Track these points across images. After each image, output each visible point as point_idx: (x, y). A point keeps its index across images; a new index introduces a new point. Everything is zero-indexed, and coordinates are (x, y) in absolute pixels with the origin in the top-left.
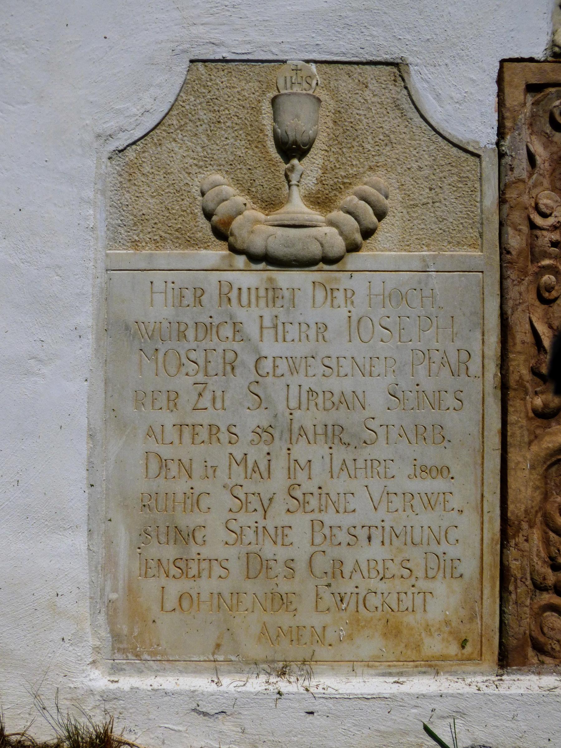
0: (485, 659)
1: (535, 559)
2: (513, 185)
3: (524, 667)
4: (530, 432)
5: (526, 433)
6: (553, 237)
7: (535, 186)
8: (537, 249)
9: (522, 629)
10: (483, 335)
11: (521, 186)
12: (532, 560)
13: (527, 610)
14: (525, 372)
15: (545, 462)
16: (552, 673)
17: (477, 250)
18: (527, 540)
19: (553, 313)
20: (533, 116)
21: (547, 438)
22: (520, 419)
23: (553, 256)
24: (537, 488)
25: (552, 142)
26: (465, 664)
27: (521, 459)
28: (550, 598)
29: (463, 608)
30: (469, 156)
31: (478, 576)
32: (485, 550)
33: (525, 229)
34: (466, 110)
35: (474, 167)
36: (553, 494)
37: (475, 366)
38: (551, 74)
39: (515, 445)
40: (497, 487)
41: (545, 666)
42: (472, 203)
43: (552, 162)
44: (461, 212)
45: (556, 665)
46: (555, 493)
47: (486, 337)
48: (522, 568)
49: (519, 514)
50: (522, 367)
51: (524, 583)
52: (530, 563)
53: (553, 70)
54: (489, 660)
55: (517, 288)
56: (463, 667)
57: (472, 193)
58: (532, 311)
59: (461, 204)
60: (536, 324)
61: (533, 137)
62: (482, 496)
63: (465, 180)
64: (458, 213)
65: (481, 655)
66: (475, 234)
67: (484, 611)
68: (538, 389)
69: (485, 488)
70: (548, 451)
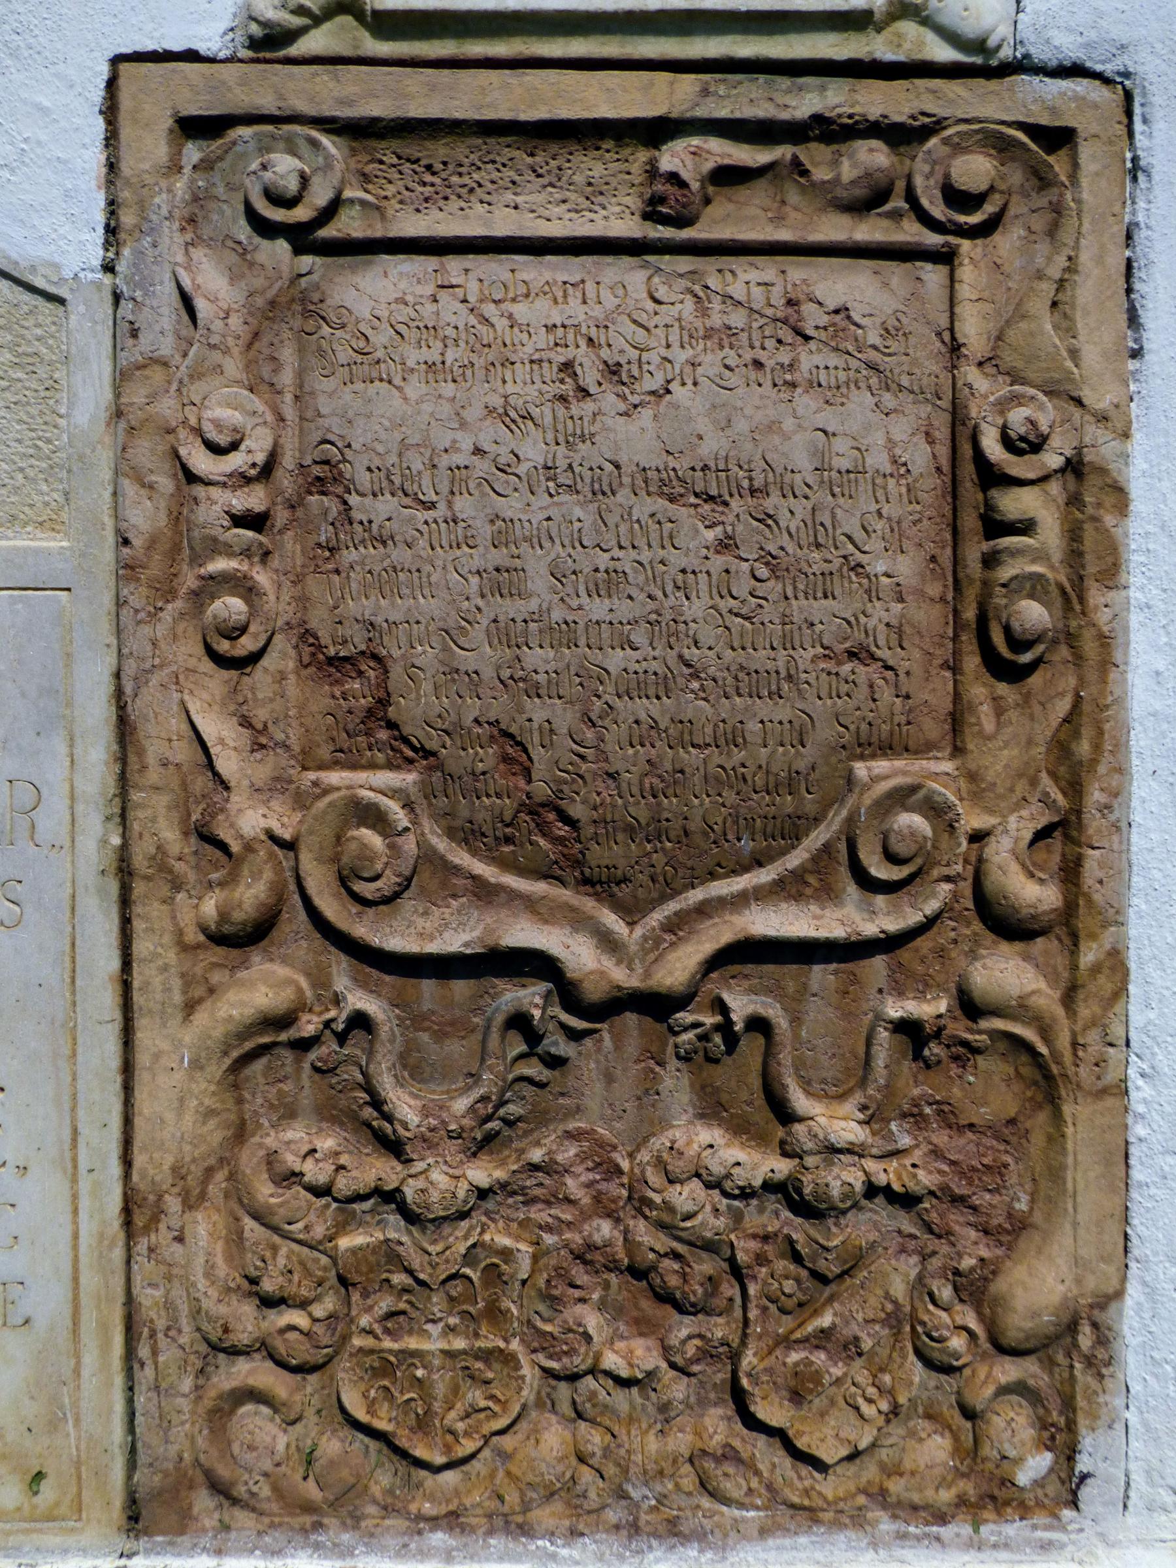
0: (88, 1520)
1: (202, 1284)
2: (138, 373)
3: (184, 1538)
4: (188, 981)
5: (176, 983)
6: (234, 502)
7: (196, 375)
8: (196, 533)
9: (173, 1450)
10: (71, 746)
11: (157, 375)
12: (194, 1285)
13: (184, 1404)
14: (170, 835)
15: (226, 1053)
16: (252, 1552)
17: (58, 536)
18: (180, 1239)
19: (253, 689)
20: (196, 199)
21: (232, 996)
22: (160, 950)
23: (237, 549)
24: (210, 1113)
25: (251, 264)
26: (40, 1531)
27: (165, 1046)
28: (250, 1373)
29: (32, 1398)
30: (39, 301)
31: (69, 1323)
32: (84, 1260)
33: (165, 483)
34: (26, 186)
35: (53, 328)
36: (259, 1126)
37: (52, 820)
38: (238, 91)
39: (150, 1011)
40: (110, 1111)
41: (233, 1535)
42: (48, 418)
43: (251, 314)
44: (19, 441)
45: (259, 1533)
46: (266, 1124)
47: (78, 751)
48: (169, 1305)
49: (158, 1178)
50: (162, 823)
51: (174, 1340)
52: (188, 1294)
53: (244, 82)
54: (99, 1522)
55: (146, 630)
56: (34, 1536)
57: (47, 394)
58: (191, 686)
59: (20, 421)
60: (198, 720)
61: (198, 254)
62: (75, 1132)
63: (30, 360)
64: (13, 444)
65: (80, 1511)
66: (55, 495)
67: (84, 1404)
68: (215, 876)
69: (81, 1113)
70: (230, 1027)
